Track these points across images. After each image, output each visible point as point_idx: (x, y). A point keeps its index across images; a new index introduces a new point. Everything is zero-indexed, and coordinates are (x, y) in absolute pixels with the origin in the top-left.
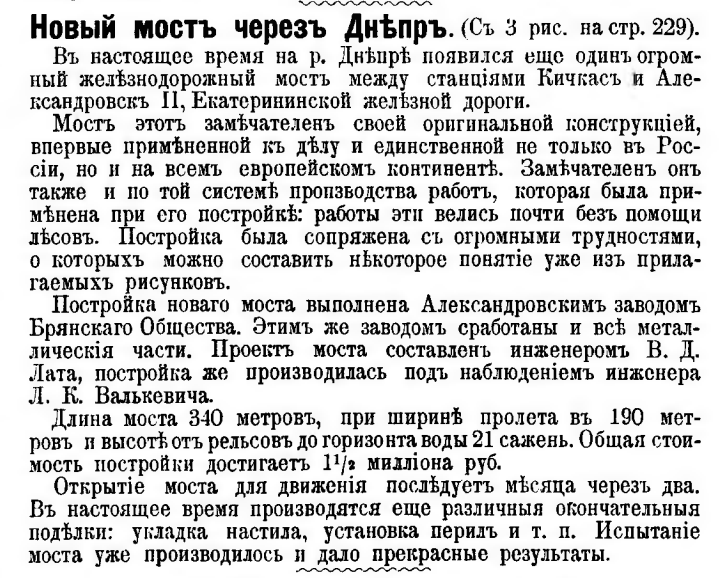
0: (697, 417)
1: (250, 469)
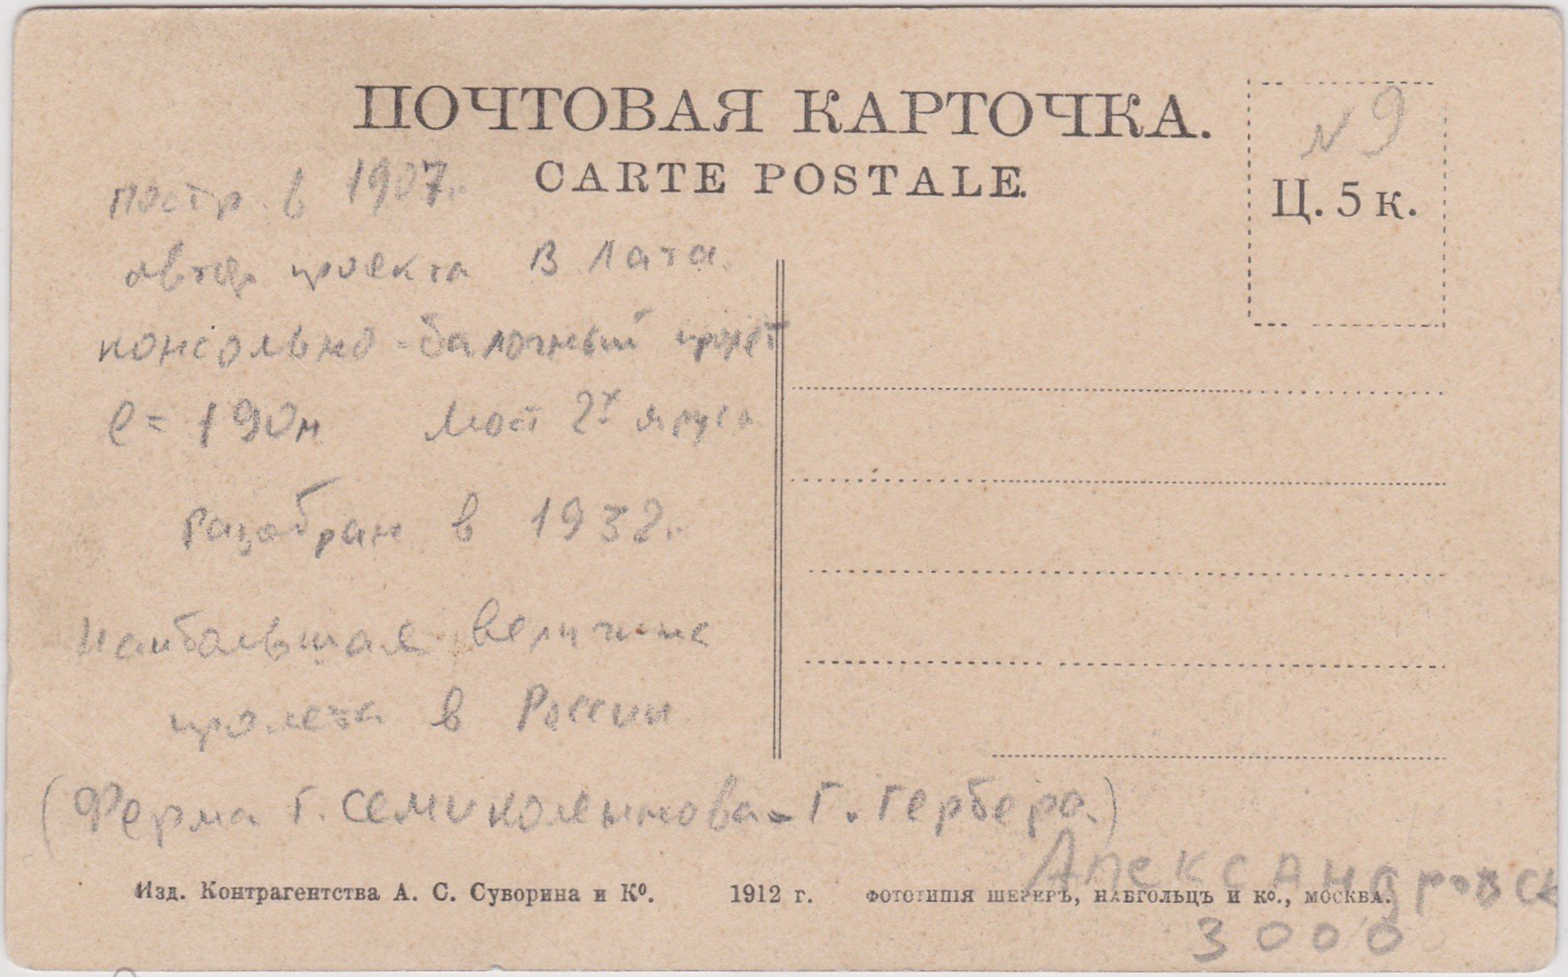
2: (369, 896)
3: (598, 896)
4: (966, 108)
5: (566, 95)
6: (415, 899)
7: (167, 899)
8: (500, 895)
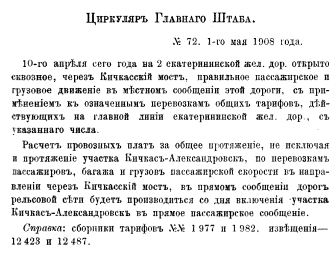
0: (328, 103)
1: (223, 76)
2: (115, 160)
3: (69, 104)
4: (167, 20)
5: (200, 17)
6: (254, 22)
7: (164, 203)
8: (31, 117)
